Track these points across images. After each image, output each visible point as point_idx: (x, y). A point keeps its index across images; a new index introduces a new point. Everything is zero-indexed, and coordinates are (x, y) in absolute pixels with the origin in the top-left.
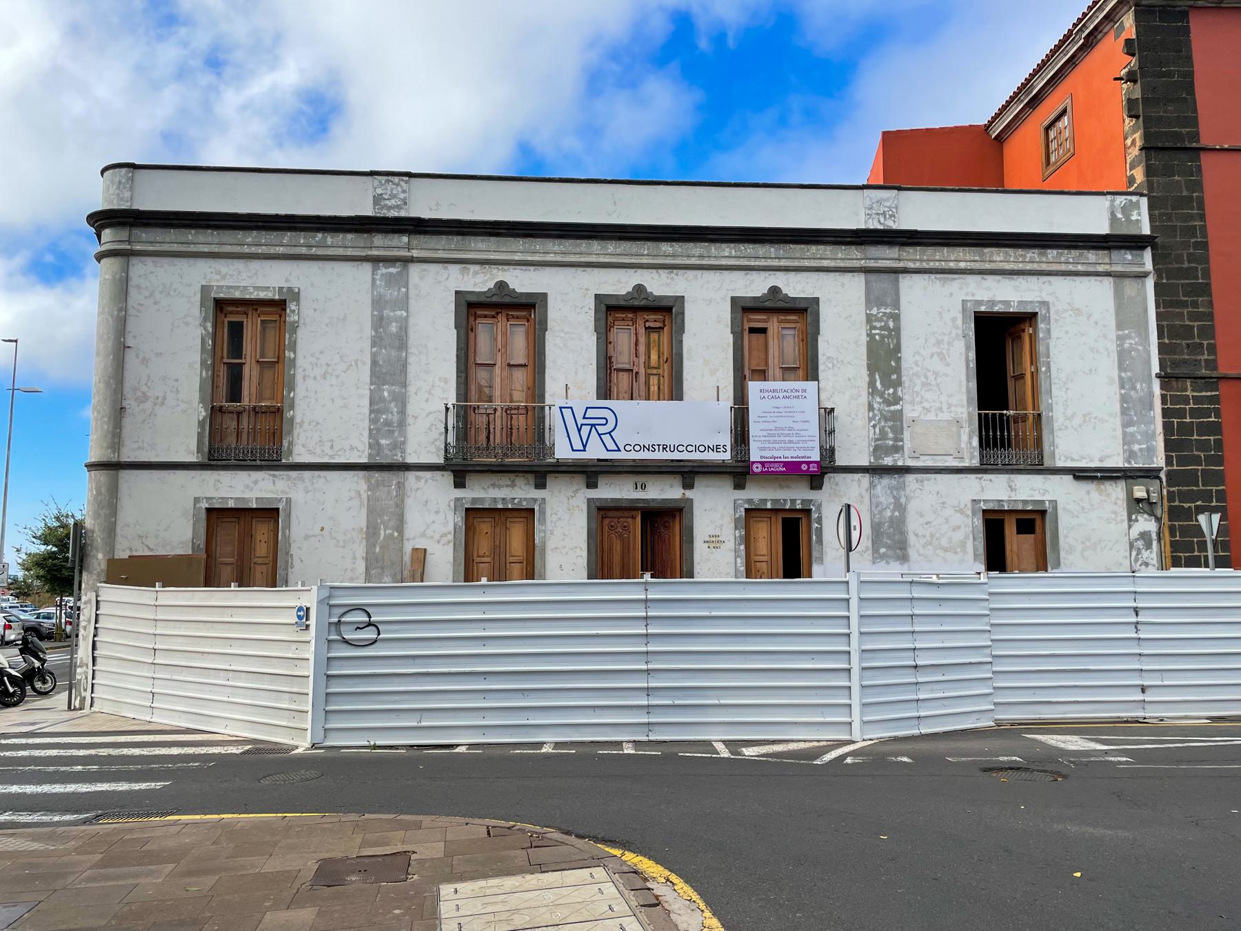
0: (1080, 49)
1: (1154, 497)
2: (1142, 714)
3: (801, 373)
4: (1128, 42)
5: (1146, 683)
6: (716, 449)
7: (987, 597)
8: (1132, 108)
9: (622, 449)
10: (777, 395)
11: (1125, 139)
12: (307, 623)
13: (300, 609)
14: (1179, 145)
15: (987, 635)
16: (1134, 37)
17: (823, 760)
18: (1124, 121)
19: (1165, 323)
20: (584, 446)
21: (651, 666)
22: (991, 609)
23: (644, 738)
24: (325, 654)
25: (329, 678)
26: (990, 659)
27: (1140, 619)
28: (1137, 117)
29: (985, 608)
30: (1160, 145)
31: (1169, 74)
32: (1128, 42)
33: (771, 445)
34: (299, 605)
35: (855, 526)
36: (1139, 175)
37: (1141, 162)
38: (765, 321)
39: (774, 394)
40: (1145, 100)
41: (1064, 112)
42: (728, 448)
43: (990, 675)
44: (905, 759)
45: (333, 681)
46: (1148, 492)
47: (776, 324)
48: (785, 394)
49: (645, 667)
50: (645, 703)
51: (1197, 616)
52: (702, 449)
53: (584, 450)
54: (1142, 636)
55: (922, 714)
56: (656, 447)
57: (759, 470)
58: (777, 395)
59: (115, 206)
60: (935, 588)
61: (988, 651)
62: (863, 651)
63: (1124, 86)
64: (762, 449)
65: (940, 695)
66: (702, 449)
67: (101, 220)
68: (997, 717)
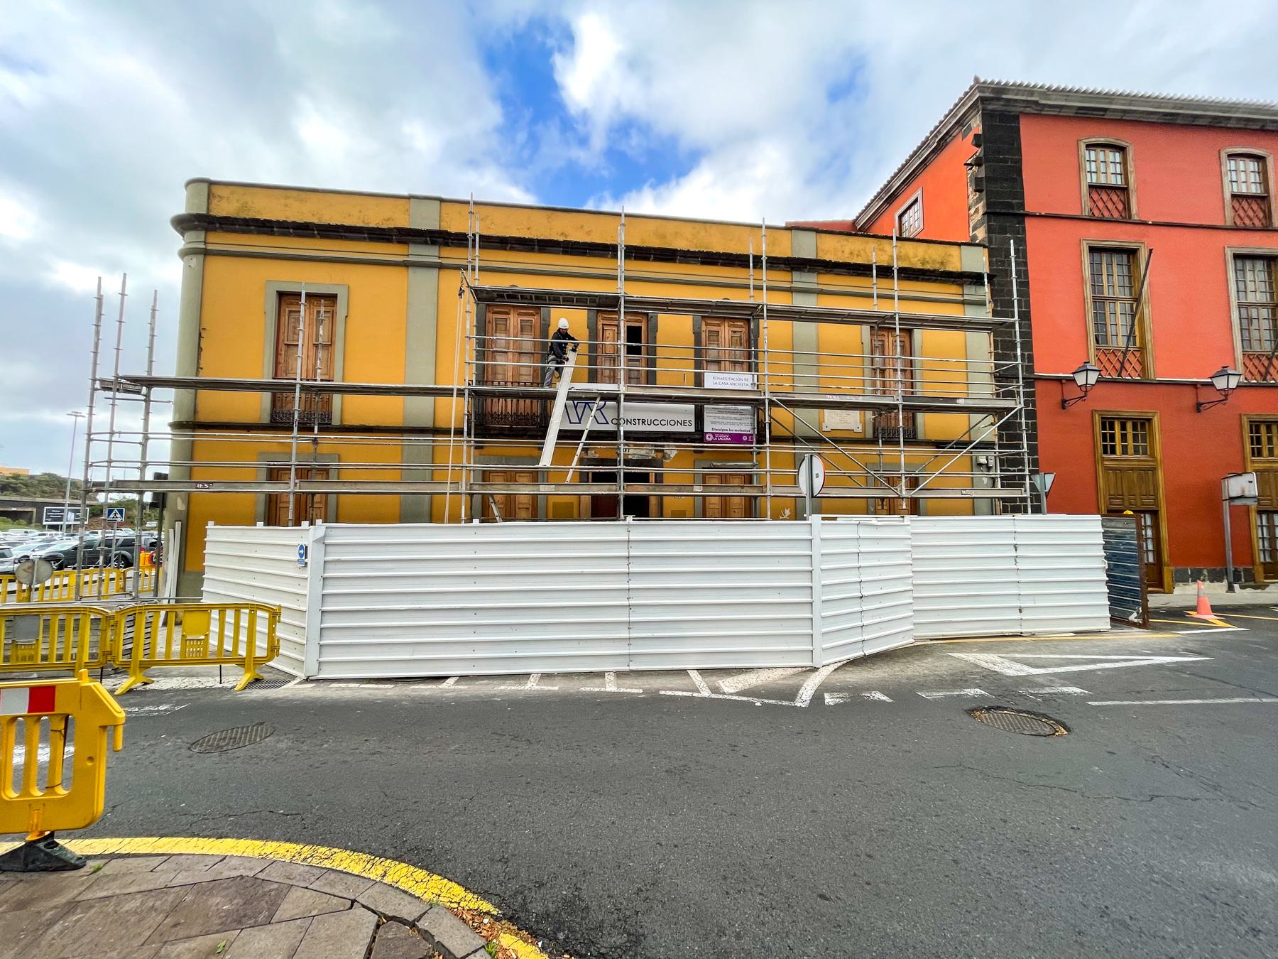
0: (932, 151)
1: (992, 463)
2: (1020, 630)
3: (745, 366)
4: (976, 136)
5: (1022, 605)
6: (684, 423)
7: (910, 536)
8: (979, 186)
9: (610, 422)
10: (726, 382)
11: (969, 209)
12: (306, 560)
13: (301, 547)
14: (1011, 211)
15: (909, 568)
16: (980, 133)
17: (804, 698)
18: (968, 197)
19: (999, 339)
20: (580, 420)
21: (632, 602)
22: (912, 546)
23: (626, 668)
24: (320, 592)
25: (325, 614)
26: (911, 588)
27: (1019, 553)
28: (980, 191)
29: (907, 546)
30: (998, 210)
31: (1005, 161)
32: (976, 136)
33: (721, 421)
34: (300, 543)
35: (817, 474)
36: (981, 234)
37: (983, 223)
38: (719, 325)
39: (724, 381)
40: (988, 179)
41: (916, 201)
42: (693, 423)
43: (911, 601)
44: (879, 696)
45: (327, 616)
46: (987, 459)
47: (727, 328)
48: (732, 381)
49: (626, 603)
50: (627, 635)
51: (1069, 551)
52: (672, 423)
53: (580, 423)
54: (1020, 567)
55: (866, 637)
56: (637, 421)
57: (711, 439)
58: (726, 382)
59: (194, 212)
60: (874, 529)
61: (910, 581)
62: (823, 586)
63: (970, 172)
64: (712, 423)
65: (878, 620)
66: (672, 423)
67: (184, 224)
68: (915, 634)
